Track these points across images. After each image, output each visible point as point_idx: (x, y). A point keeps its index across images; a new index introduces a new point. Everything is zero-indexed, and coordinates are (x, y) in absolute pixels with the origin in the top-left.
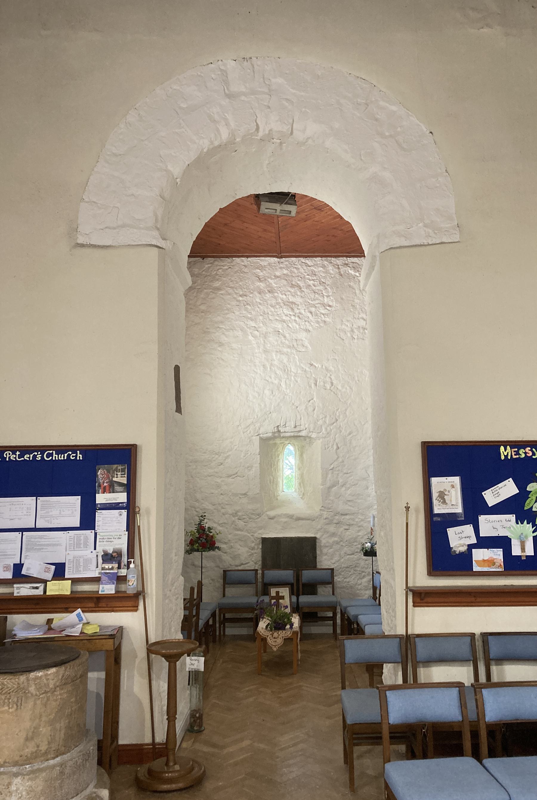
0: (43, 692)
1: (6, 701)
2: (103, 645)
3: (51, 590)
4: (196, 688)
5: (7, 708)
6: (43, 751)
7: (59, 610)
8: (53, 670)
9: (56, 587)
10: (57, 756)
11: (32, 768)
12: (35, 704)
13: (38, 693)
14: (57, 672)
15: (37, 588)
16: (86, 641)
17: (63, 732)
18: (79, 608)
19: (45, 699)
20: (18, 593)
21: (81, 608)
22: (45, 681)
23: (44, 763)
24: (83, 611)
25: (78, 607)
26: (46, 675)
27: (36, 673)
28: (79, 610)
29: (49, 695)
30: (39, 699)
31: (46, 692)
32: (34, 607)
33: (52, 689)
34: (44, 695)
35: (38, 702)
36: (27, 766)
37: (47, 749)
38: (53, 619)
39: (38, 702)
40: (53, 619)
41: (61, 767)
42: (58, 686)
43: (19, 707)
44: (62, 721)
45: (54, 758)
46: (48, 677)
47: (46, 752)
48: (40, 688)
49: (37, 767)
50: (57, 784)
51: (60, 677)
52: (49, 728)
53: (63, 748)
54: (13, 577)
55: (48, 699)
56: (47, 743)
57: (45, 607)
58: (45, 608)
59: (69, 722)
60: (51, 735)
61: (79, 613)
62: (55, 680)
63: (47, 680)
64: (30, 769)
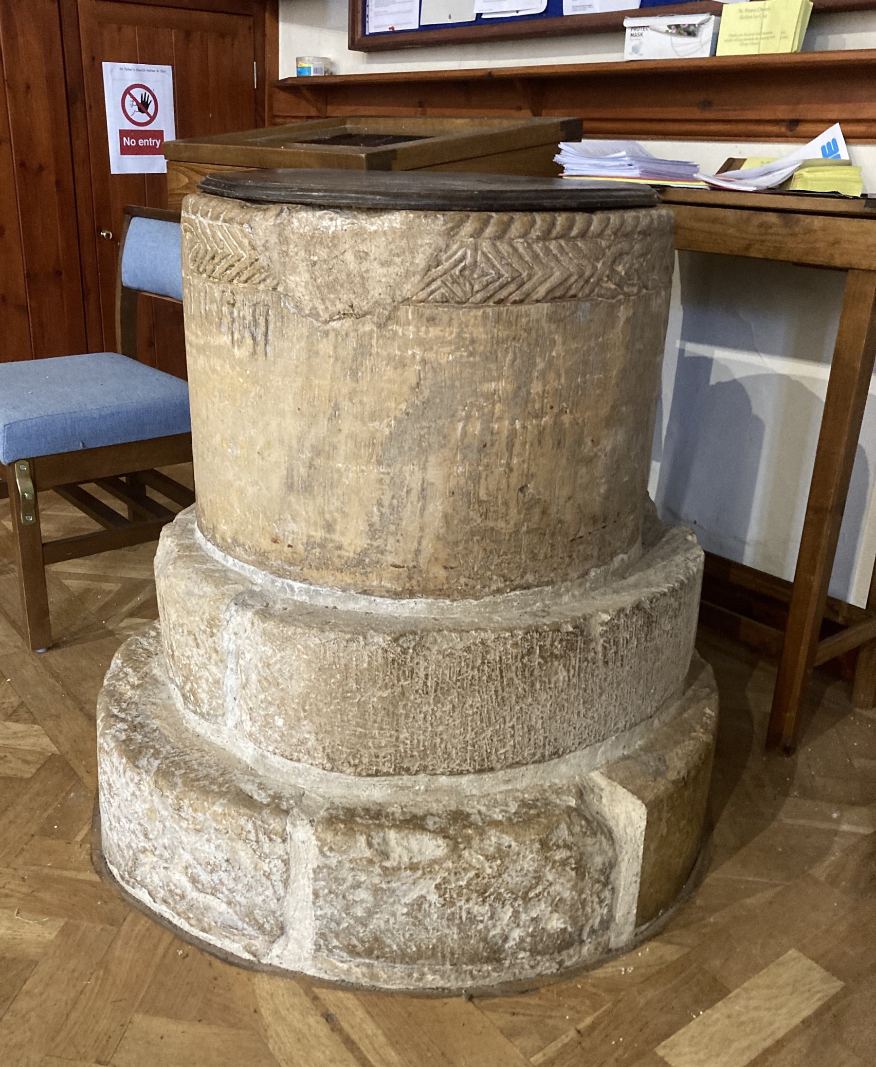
0: (340, 306)
1: (225, 309)
2: (836, 242)
3: (732, 38)
4: (362, 942)
5: (226, 339)
6: (349, 553)
7: (769, 128)
8: (396, 220)
9: (752, 26)
10: (412, 594)
11: (311, 597)
12: (312, 352)
13: (321, 307)
14: (408, 233)
15: (690, 32)
16: (772, 218)
17: (437, 508)
18: (833, 122)
19: (352, 343)
20: (635, 50)
21: (841, 122)
22: (352, 263)
23: (351, 598)
24: (847, 137)
25: (834, 116)
26: (359, 235)
27: (320, 218)
28: (835, 132)
29: (367, 328)
30: (327, 333)
31: (352, 313)
32: (698, 114)
33: (377, 303)
34: (348, 323)
35: (325, 347)
36: (297, 585)
37: (365, 552)
38: (745, 160)
39: (325, 347)
40: (745, 160)
41: (396, 640)
42: (406, 301)
43: (260, 349)
44: (432, 459)
45: (397, 595)
46: (363, 247)
47: (360, 563)
48: (331, 287)
49: (330, 602)
50: (375, 696)
51: (421, 260)
52: (374, 472)
53: (442, 573)
54: (641, 6)
55: (363, 349)
56: (363, 527)
57: (732, 115)
58: (729, 121)
59: (475, 478)
60: (380, 504)
61: (834, 141)
62: (393, 270)
63: (362, 256)
64: (305, 598)
